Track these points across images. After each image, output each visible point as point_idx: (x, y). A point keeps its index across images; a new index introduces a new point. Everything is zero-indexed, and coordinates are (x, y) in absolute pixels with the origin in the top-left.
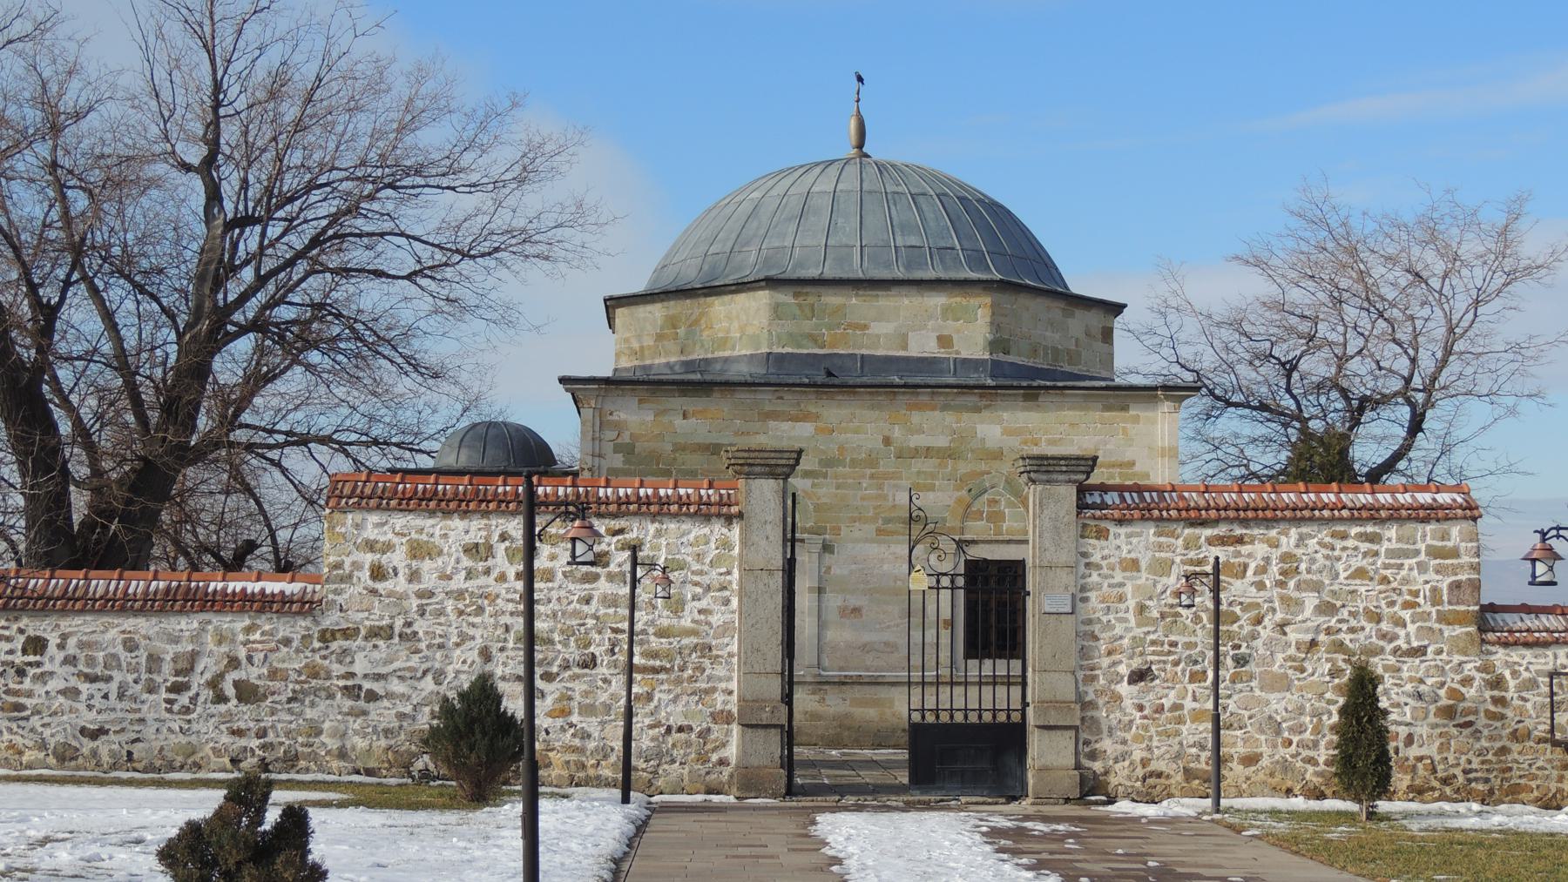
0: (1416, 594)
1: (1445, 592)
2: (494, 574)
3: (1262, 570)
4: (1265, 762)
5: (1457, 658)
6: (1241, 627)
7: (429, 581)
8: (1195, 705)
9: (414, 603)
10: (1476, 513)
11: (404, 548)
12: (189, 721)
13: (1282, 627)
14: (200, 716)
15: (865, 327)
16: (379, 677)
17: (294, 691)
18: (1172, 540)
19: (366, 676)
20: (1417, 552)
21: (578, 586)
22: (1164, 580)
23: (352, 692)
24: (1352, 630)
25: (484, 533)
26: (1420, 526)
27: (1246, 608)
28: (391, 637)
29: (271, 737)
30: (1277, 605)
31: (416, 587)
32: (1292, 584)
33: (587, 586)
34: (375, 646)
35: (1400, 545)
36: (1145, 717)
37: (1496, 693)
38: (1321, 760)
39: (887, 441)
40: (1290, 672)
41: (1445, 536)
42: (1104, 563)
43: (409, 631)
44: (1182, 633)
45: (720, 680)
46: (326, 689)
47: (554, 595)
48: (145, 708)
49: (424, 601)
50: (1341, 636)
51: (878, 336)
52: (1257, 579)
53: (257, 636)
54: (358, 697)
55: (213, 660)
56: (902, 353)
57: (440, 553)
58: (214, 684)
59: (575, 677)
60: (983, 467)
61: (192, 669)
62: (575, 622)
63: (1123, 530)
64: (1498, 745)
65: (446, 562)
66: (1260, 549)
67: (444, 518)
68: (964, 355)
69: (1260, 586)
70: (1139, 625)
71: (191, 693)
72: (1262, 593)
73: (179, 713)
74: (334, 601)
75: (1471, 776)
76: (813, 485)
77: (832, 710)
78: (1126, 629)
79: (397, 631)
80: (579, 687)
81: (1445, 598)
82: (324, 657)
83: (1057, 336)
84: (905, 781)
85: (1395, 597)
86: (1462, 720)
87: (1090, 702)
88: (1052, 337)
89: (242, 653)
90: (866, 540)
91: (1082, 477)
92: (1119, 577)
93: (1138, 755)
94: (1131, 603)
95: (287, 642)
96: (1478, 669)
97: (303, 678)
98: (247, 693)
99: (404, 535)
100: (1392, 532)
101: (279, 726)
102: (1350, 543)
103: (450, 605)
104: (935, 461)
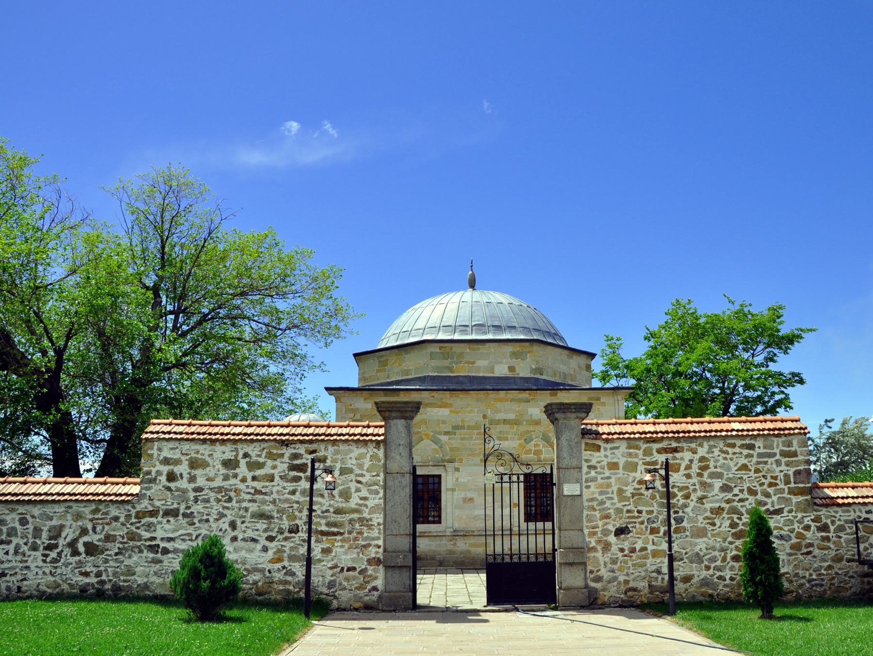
0: (775, 478)
1: (792, 477)
2: (240, 477)
3: (688, 467)
4: (695, 580)
5: (800, 515)
6: (678, 500)
7: (201, 482)
8: (654, 547)
9: (192, 495)
10: (806, 431)
11: (187, 462)
12: (56, 568)
13: (701, 500)
14: (63, 564)
15: (474, 363)
16: (170, 540)
17: (119, 548)
18: (637, 451)
19: (162, 539)
20: (775, 455)
21: (289, 484)
22: (634, 474)
23: (153, 549)
24: (741, 500)
25: (234, 453)
26: (775, 439)
27: (681, 489)
28: (177, 515)
29: (104, 577)
30: (697, 487)
31: (193, 485)
32: (706, 474)
33: (294, 484)
34: (168, 521)
35: (765, 451)
36: (625, 556)
37: (824, 534)
38: (728, 577)
39: (485, 417)
40: (708, 526)
41: (790, 444)
42: (598, 465)
43: (188, 511)
44: (645, 505)
45: (373, 539)
46: (139, 547)
47: (275, 489)
48: (30, 559)
49: (198, 494)
50: (735, 504)
51: (480, 367)
52: (687, 472)
53: (99, 516)
54: (157, 552)
55: (72, 530)
56: (491, 375)
57: (208, 465)
58: (72, 544)
59: (286, 539)
60: (531, 428)
61: (60, 535)
62: (286, 505)
63: (609, 446)
64: (826, 564)
65: (210, 471)
66: (687, 455)
67: (211, 445)
68: (521, 375)
69: (688, 476)
70: (620, 501)
71: (58, 550)
72: (689, 481)
73: (51, 562)
74: (145, 494)
75: (813, 583)
76: (449, 439)
77: (460, 549)
78: (612, 504)
79: (181, 511)
80: (288, 545)
81: (792, 480)
82: (138, 528)
83: (565, 368)
84: (480, 600)
85: (763, 480)
86: (805, 551)
87: (593, 548)
88: (563, 368)
89: (90, 526)
90: (475, 465)
91: (583, 415)
92: (607, 473)
93: (622, 578)
94: (615, 489)
95: (116, 519)
96: (812, 520)
97: (125, 540)
98: (91, 549)
99: (187, 454)
100: (759, 443)
101: (109, 570)
102: (737, 450)
103: (212, 495)
104: (508, 426)
